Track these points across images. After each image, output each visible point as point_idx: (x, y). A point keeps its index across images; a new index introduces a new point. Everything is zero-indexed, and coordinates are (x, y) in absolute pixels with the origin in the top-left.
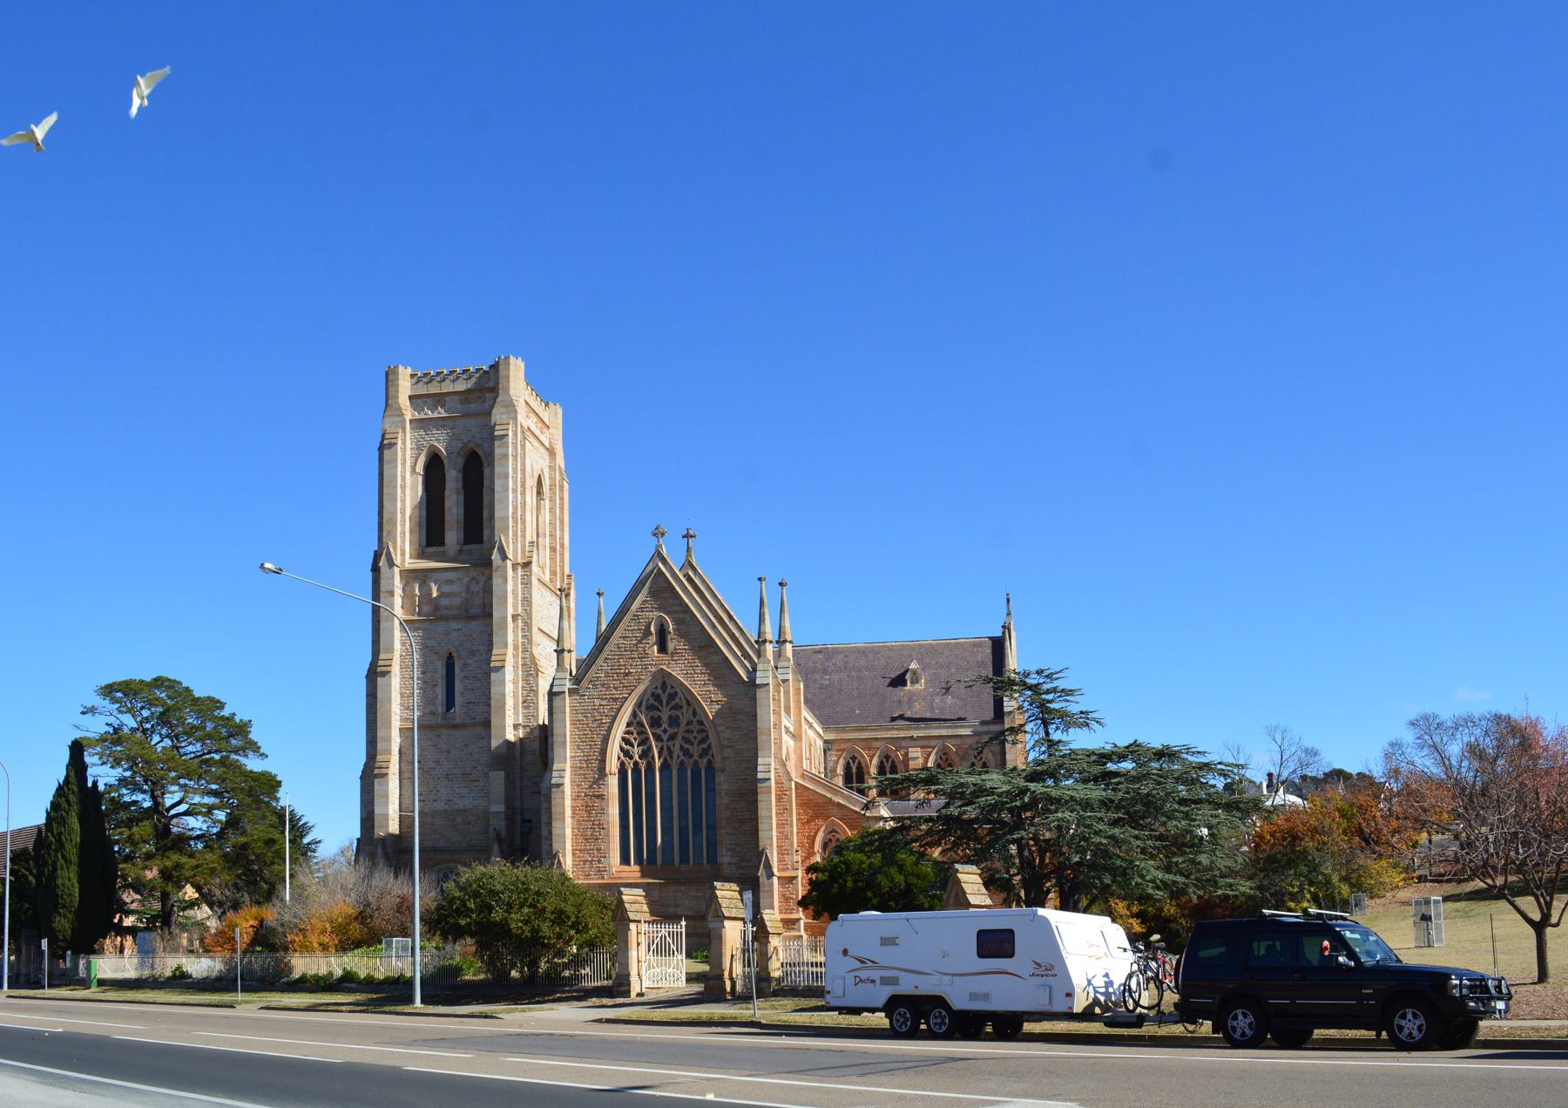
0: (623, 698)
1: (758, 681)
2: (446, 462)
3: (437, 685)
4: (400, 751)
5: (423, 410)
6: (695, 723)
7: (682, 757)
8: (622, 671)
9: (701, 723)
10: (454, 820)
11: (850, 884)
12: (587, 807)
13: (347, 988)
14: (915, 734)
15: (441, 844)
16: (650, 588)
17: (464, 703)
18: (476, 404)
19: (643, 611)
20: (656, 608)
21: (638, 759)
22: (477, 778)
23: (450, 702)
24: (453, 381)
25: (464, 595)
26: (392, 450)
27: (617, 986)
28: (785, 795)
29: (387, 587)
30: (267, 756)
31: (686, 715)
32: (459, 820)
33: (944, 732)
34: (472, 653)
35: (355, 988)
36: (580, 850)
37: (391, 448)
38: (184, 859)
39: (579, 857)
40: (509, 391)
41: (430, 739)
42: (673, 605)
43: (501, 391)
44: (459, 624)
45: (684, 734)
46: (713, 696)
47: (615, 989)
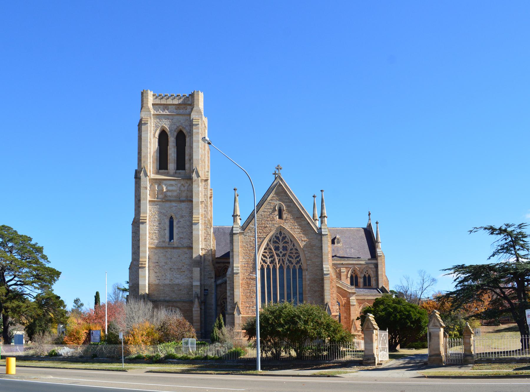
0: (264, 237)
1: (323, 233)
2: (169, 134)
3: (166, 230)
4: (149, 257)
5: (159, 110)
6: (294, 250)
7: (288, 264)
8: (263, 226)
9: (297, 250)
10: (174, 288)
11: (399, 316)
12: (247, 283)
13: (170, 362)
14: (344, 262)
15: (167, 298)
16: (276, 191)
17: (178, 238)
18: (182, 110)
19: (272, 201)
20: (278, 200)
21: (269, 264)
22: (184, 271)
23: (171, 237)
24: (172, 99)
25: (178, 191)
26: (146, 125)
27: (366, 360)
28: (333, 281)
29: (144, 185)
30: (50, 262)
31: (290, 247)
32: (176, 288)
33: (354, 262)
34: (182, 217)
35: (175, 362)
36: (244, 302)
37: (145, 125)
38: (21, 304)
39: (244, 305)
40: (199, 106)
41: (163, 253)
42: (285, 199)
43: (195, 105)
44: (176, 204)
45: (289, 254)
46: (302, 238)
47: (364, 362)
